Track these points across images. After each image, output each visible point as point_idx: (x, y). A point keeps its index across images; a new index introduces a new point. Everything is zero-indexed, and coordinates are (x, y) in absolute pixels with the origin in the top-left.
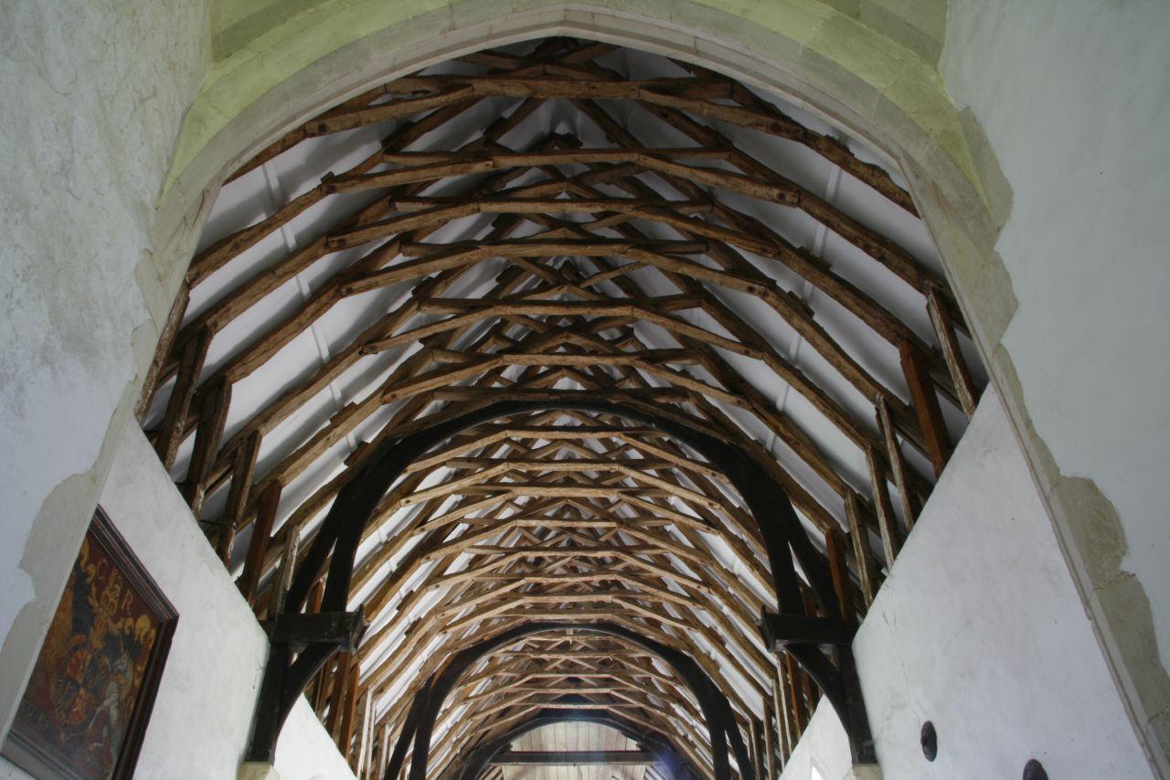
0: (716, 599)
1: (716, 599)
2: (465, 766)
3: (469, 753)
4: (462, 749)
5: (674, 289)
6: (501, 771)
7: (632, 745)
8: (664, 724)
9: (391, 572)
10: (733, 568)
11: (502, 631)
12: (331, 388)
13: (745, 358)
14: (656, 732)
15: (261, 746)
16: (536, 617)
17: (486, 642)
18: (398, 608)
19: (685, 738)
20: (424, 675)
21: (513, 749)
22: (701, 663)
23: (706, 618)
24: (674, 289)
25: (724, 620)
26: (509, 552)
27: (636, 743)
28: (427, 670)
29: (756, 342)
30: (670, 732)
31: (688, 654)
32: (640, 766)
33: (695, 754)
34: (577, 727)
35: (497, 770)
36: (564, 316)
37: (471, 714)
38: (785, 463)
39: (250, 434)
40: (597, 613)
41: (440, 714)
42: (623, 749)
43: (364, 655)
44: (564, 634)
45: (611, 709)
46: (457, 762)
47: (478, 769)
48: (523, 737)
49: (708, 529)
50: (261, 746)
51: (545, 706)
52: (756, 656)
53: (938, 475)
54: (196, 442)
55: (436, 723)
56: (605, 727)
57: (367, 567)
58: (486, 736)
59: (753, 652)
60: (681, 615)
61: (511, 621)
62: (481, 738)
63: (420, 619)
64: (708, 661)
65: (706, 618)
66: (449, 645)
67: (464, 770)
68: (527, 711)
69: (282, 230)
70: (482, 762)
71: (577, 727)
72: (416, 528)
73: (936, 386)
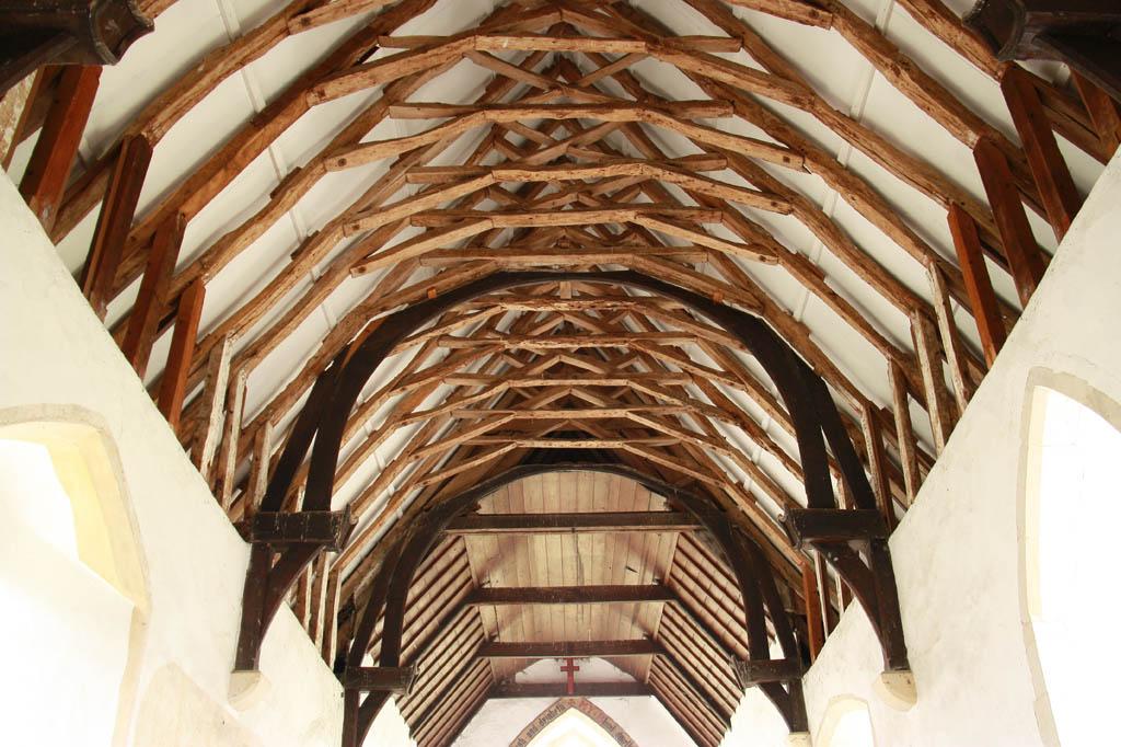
0: (814, 184)
1: (814, 184)
2: (410, 535)
3: (415, 516)
4: (405, 512)
5: (697, 93)
6: (479, 613)
7: (659, 503)
8: (705, 466)
9: (255, 113)
10: (850, 109)
11: (458, 282)
12: (323, 307)
13: (762, 264)
14: (697, 482)
15: (247, 657)
16: (516, 262)
17: (432, 300)
18: (273, 195)
19: (740, 486)
20: (331, 349)
21: (481, 512)
22: (778, 326)
23: (795, 231)
24: (697, 93)
25: (832, 230)
26: (497, 382)
27: (664, 499)
28: (335, 340)
29: (800, 147)
30: (716, 477)
31: (757, 316)
32: (666, 535)
33: (755, 508)
34: (577, 480)
35: (458, 547)
36: (563, 122)
37: (416, 447)
38: (818, 339)
39: (171, 221)
40: (608, 252)
41: (354, 412)
42: (646, 510)
43: (211, 263)
44: (551, 297)
45: (627, 448)
46: (397, 529)
47: (429, 538)
48: (496, 494)
49: (813, 15)
50: (247, 657)
51: (528, 444)
52: (883, 279)
53: (1025, 304)
54: (141, 290)
55: (348, 425)
56: (617, 478)
57: (201, 69)
58: (446, 489)
59: (878, 272)
60: (722, 366)
61: (472, 267)
62: (434, 495)
63: (298, 169)
64: (789, 323)
65: (795, 231)
66: (372, 302)
67: (408, 540)
68: (502, 451)
69: (323, 307)
70: (436, 528)
71: (577, 480)
72: (294, 16)
73: (1021, 196)
